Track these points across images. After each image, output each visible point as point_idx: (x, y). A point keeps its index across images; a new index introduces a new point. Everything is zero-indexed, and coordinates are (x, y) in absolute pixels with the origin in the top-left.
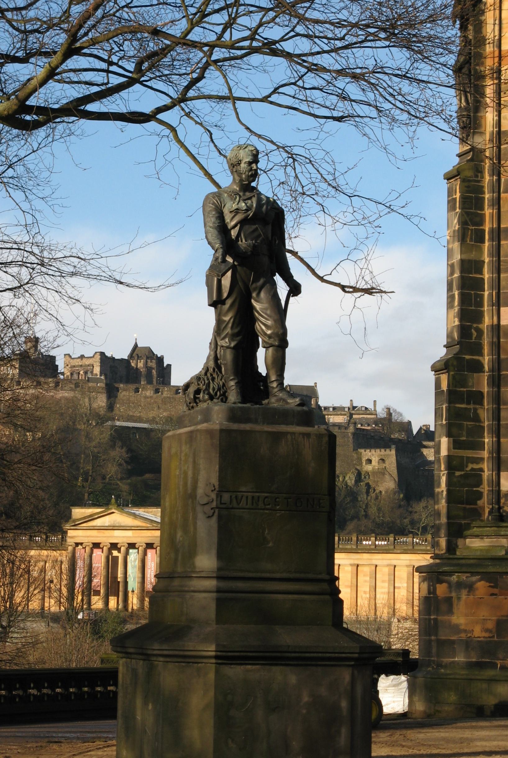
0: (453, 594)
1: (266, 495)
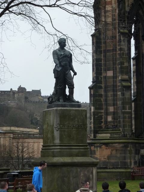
0: (96, 149)
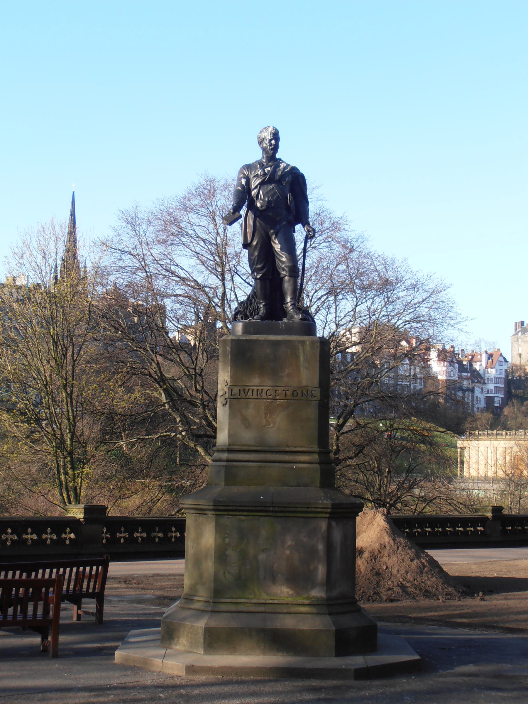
1: (268, 388)
